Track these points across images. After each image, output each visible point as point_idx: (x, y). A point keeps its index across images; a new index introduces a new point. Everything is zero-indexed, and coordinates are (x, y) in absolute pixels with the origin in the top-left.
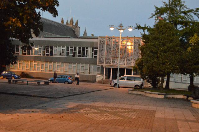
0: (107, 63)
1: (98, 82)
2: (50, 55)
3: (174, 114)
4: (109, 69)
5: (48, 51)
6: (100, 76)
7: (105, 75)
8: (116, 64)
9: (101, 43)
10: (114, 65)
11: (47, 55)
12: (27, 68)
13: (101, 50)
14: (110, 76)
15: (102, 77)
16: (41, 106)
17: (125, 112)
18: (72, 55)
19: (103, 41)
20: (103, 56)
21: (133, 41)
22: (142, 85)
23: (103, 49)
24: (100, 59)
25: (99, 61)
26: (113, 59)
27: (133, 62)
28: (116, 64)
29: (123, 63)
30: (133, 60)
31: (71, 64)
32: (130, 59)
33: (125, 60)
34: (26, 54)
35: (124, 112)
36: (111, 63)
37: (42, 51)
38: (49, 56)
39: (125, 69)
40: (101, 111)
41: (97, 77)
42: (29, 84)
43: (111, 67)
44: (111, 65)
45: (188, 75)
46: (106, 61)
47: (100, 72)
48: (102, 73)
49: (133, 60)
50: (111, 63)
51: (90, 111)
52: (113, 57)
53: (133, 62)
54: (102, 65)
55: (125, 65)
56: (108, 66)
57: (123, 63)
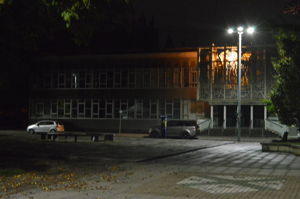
0: (215, 97)
1: (202, 132)
2: (100, 117)
3: (297, 193)
4: (221, 107)
6: (203, 121)
7: (212, 120)
11: (101, 86)
14: (223, 120)
15: (208, 122)
17: (262, 181)
21: (264, 52)
22: (286, 134)
30: (265, 89)
33: (250, 89)
34: (64, 86)
35: (260, 181)
38: (99, 118)
40: (219, 179)
42: (74, 137)
43: (224, 103)
46: (213, 93)
48: (208, 116)
49: (265, 89)
51: (199, 180)
54: (207, 100)
56: (218, 102)
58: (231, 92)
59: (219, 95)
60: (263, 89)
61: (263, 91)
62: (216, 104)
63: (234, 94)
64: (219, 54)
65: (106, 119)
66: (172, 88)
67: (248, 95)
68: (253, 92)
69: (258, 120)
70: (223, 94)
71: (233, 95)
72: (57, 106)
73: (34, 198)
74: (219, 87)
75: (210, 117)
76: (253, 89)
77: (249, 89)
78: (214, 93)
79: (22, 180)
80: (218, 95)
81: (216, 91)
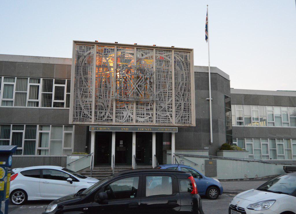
5: (59, 96)
8: (127, 121)
9: (81, 59)
10: (123, 122)
11: (56, 104)
12: (65, 146)
13: (81, 82)
16: (267, 177)
18: (36, 100)
19: (86, 54)
20: (86, 97)
23: (89, 76)
24: (77, 108)
25: (76, 115)
26: (117, 107)
27: (174, 116)
28: (127, 121)
29: (147, 118)
30: (174, 109)
31: (57, 129)
32: (165, 105)
33: (152, 109)
36: (114, 118)
37: (41, 92)
39: (110, 134)
41: (68, 162)
44: (114, 123)
45: (122, 144)
47: (72, 148)
50: (114, 118)
52: (116, 100)
53: (174, 116)
55: (154, 123)
57: (147, 118)
58: (124, 112)
59: (106, 118)
60: (170, 110)
61: (170, 113)
62: (101, 129)
63: (129, 116)
64: (106, 55)
65: (52, 107)
66: (112, 69)
67: (150, 118)
68: (156, 114)
69: (120, 146)
70: (111, 116)
71: (128, 117)
72: (152, 139)
73: (208, 5)
74: (106, 105)
75: (88, 151)
76: (156, 110)
77: (151, 109)
78: (98, 113)
79: (108, 59)
80: (104, 116)
81: (101, 111)
